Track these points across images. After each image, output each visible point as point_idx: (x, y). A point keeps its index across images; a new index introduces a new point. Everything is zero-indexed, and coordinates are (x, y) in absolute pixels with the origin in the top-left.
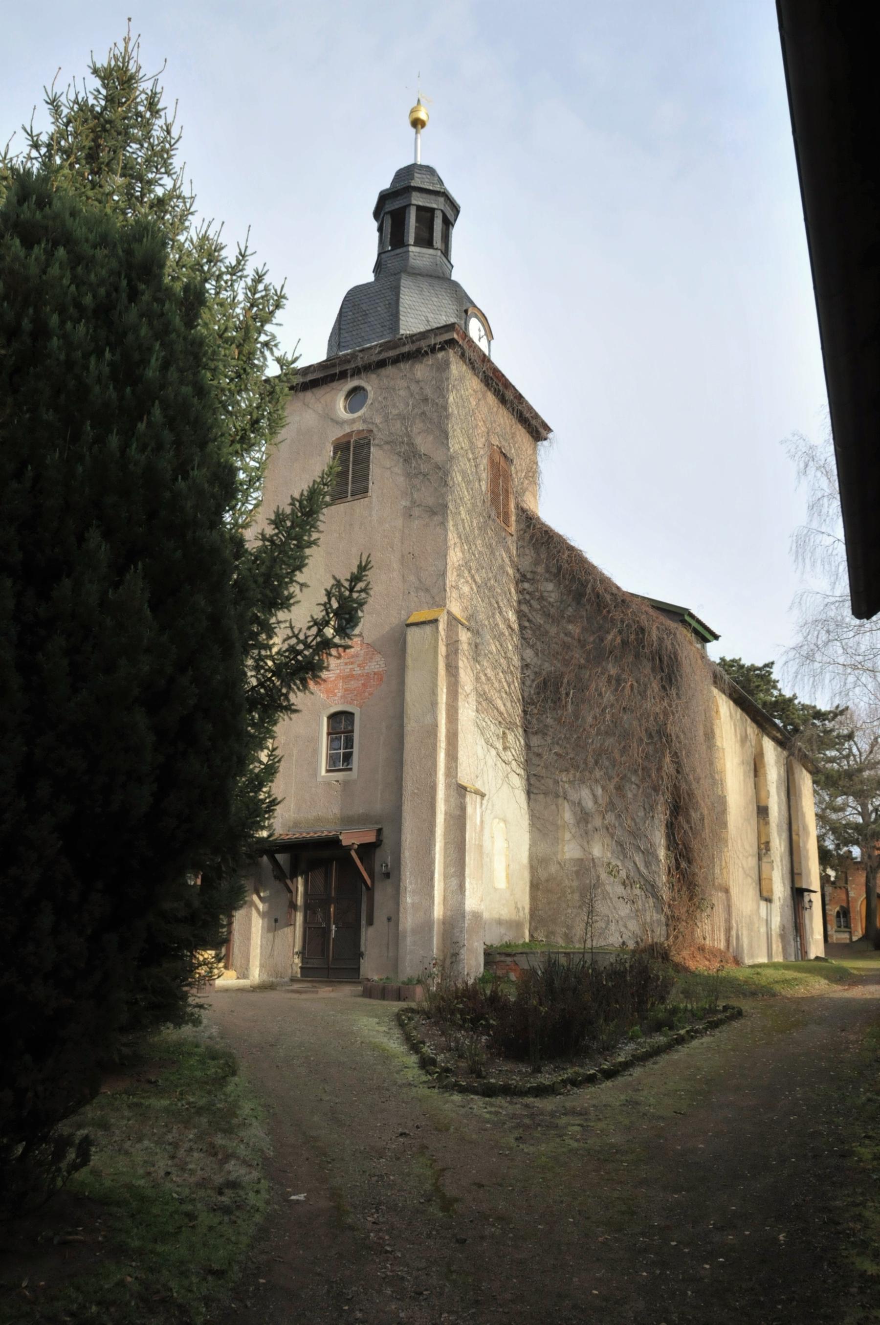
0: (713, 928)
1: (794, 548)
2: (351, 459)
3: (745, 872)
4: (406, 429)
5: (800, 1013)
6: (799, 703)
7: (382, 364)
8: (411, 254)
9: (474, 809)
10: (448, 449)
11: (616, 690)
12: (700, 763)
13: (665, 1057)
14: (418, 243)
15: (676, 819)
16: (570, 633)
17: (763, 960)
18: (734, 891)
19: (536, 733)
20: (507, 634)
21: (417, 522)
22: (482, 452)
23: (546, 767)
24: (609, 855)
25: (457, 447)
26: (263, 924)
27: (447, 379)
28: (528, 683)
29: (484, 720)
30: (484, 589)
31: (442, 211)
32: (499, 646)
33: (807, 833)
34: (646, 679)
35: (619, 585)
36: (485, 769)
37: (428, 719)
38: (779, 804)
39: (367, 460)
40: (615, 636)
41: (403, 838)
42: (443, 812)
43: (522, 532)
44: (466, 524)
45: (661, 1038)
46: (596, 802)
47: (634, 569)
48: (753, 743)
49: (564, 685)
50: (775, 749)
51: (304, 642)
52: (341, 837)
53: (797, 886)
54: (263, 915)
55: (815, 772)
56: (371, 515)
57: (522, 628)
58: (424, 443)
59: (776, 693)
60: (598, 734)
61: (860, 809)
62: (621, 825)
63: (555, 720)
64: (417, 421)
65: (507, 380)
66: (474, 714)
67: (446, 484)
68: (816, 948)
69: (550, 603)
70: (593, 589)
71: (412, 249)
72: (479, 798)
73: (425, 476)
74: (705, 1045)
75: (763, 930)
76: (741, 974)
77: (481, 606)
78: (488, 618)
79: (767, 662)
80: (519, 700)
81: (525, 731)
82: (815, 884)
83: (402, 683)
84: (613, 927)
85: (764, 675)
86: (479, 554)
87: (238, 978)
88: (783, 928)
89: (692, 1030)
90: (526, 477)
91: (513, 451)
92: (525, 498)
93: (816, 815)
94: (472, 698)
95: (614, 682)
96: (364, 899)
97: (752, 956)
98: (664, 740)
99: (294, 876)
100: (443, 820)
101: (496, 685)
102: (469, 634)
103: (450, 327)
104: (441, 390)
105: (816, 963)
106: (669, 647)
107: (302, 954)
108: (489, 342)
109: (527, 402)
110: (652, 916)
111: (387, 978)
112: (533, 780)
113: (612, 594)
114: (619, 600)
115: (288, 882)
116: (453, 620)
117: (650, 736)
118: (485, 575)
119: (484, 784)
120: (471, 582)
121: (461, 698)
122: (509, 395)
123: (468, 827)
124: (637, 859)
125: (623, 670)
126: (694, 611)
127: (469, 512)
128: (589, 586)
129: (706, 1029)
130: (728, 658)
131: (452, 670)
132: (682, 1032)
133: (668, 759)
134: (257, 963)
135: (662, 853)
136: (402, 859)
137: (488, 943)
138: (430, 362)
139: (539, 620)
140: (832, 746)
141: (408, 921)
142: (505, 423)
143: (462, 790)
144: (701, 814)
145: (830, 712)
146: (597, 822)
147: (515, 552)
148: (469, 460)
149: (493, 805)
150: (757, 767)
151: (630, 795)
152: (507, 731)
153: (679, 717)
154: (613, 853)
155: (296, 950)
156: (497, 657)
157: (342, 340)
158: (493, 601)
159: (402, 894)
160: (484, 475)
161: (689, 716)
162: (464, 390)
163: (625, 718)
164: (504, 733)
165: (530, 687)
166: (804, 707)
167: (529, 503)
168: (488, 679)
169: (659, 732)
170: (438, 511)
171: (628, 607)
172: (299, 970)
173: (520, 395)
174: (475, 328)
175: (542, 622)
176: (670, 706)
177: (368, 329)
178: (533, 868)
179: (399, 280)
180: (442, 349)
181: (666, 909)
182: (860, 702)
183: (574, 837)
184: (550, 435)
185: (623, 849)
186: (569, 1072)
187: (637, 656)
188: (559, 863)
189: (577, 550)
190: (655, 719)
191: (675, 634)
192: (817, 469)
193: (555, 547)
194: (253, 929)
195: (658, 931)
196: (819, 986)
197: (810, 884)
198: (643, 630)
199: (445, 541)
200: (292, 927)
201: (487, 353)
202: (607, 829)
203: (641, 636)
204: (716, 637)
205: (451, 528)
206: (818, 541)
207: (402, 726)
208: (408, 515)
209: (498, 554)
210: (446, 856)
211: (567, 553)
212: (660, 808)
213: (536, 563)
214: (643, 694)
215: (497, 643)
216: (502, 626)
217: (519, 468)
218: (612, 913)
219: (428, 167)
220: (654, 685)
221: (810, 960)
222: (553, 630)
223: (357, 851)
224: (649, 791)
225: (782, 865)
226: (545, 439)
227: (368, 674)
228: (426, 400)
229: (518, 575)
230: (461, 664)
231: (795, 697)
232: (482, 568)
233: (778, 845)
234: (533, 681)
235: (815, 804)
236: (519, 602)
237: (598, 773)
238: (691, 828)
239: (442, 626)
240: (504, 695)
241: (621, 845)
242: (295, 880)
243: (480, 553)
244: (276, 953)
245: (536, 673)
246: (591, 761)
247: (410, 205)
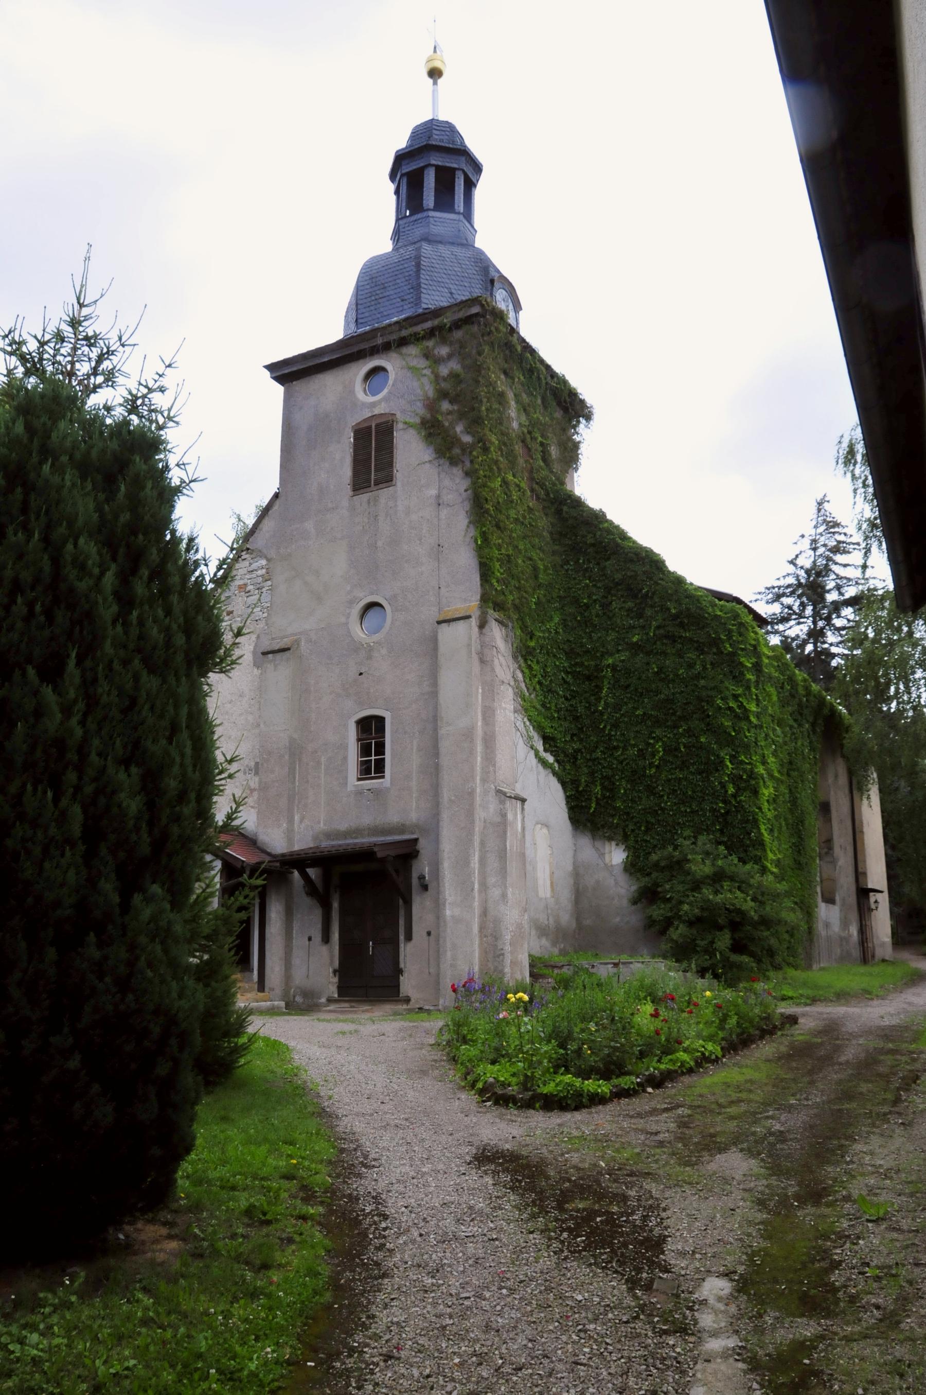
2: (373, 445)
14: (438, 207)
56: (396, 506)
72: (519, 803)
96: (402, 913)
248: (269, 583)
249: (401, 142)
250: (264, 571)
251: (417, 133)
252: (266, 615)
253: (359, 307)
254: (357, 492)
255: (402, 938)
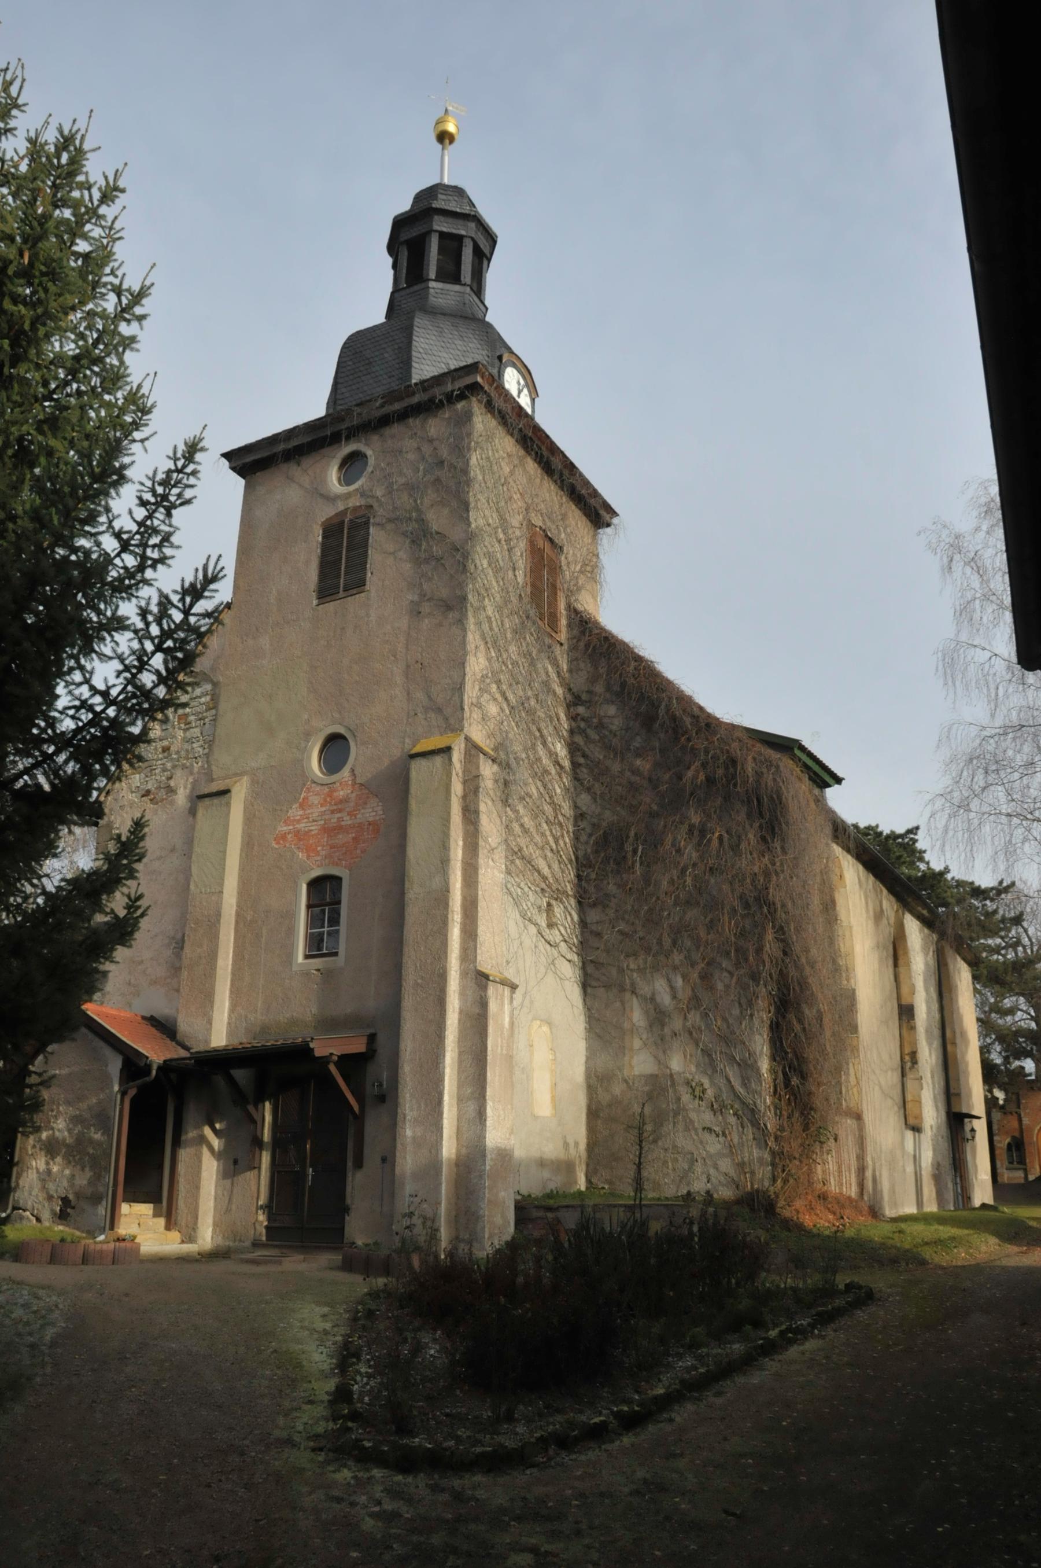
0: (840, 1167)
1: (940, 667)
2: (345, 544)
3: (883, 1092)
4: (415, 501)
5: (960, 1296)
6: (953, 878)
7: (384, 422)
8: (431, 291)
9: (500, 1007)
10: (469, 524)
11: (699, 844)
12: (815, 941)
13: (740, 1380)
14: (441, 277)
15: (784, 1017)
16: (638, 770)
17: (911, 1209)
18: (868, 1117)
19: (594, 905)
20: (553, 771)
21: (426, 621)
22: (518, 533)
23: (608, 951)
24: (693, 1069)
25: (481, 522)
26: (218, 1166)
27: (469, 435)
28: (584, 838)
29: (519, 886)
30: (519, 709)
31: (473, 239)
32: (542, 789)
33: (966, 1041)
34: (740, 829)
35: (702, 703)
36: (520, 952)
37: (437, 882)
38: (928, 1002)
39: (365, 544)
40: (697, 771)
41: (402, 1046)
42: (457, 1010)
43: (575, 641)
44: (494, 624)
45: (736, 1346)
46: (674, 997)
47: (727, 686)
48: (892, 920)
49: (631, 839)
50: (921, 931)
51: (105, 694)
52: (312, 1045)
53: (955, 1110)
54: (218, 1156)
55: (974, 963)
56: (368, 615)
57: (575, 765)
58: (437, 519)
59: (922, 866)
60: (676, 904)
61: (1033, 1014)
62: (708, 1026)
63: (619, 886)
64: (429, 492)
65: (552, 443)
66: (502, 876)
67: (465, 569)
68: (982, 1193)
69: (611, 732)
70: (668, 708)
71: (432, 284)
72: (507, 991)
73: (438, 560)
74: (807, 1355)
75: (910, 1169)
76: (877, 1232)
77: (514, 732)
78: (526, 749)
79: (910, 827)
80: (570, 861)
81: (579, 903)
82: (978, 1108)
83: (403, 836)
84: (699, 1168)
85: (908, 843)
86: (512, 664)
87: (183, 1242)
88: (937, 1166)
89: (789, 1330)
90: (581, 572)
91: (563, 535)
92: (580, 598)
93: (979, 1020)
94: (500, 855)
95: (696, 833)
96: (351, 1131)
97: (895, 1205)
98: (765, 910)
99: (259, 1100)
100: (456, 1021)
101: (538, 839)
102: (495, 768)
103: (472, 368)
104: (460, 449)
105: (981, 1213)
106: (770, 783)
107: (268, 1208)
108: (533, 400)
109: (581, 475)
110: (751, 1153)
111: (376, 1243)
112: (590, 969)
113: (693, 716)
114: (703, 724)
115: (251, 1108)
116: (473, 749)
117: (747, 906)
118: (521, 693)
119: (518, 972)
120: (500, 697)
121: (482, 853)
122: (556, 463)
123: (491, 1030)
124: (731, 1074)
125: (709, 816)
126: (806, 743)
127: (499, 609)
128: (663, 707)
129: (813, 1326)
130: (862, 825)
131: (471, 815)
132: (773, 1333)
133: (770, 936)
134: (210, 1220)
135: (765, 1065)
136: (401, 1074)
137: (525, 1192)
138: (447, 416)
139: (598, 754)
140: (994, 934)
141: (408, 1162)
142: (552, 500)
143: (482, 979)
144: (819, 1011)
145: (992, 889)
146: (677, 1024)
147: (565, 667)
148: (499, 541)
149: (532, 1002)
150: (896, 951)
151: (720, 986)
152: (554, 902)
153: (785, 879)
154: (697, 1066)
155: (260, 1203)
156: (538, 803)
157: (338, 397)
158: (534, 728)
159: (400, 1124)
160: (521, 564)
161: (798, 877)
162: (492, 450)
163: (713, 881)
164: (549, 905)
165: (587, 843)
166: (960, 884)
167: (585, 603)
168: (526, 831)
169: (757, 899)
170: (454, 606)
171: (715, 733)
172: (264, 1231)
173: (572, 464)
174: (511, 379)
175: (601, 757)
176: (774, 864)
177: (371, 381)
178: (591, 1089)
179: (412, 319)
180: (462, 397)
181: (771, 1143)
182: (1030, 875)
183: (645, 1045)
184: (615, 520)
185: (712, 1060)
186: (556, 1423)
187: (727, 798)
188: (626, 1081)
189: (647, 661)
190: (753, 881)
191: (778, 767)
192: (965, 564)
193: (618, 658)
194: (204, 1174)
195: (759, 1175)
196: (986, 1248)
197: (970, 1106)
198: (734, 762)
199: (464, 643)
200: (256, 1171)
201: (529, 411)
202: (691, 1033)
203: (731, 770)
204: (839, 780)
205: (472, 626)
206: (969, 658)
207: (402, 894)
208: (416, 613)
209: (539, 666)
210: (461, 1070)
211: (633, 664)
212: (761, 1003)
213: (593, 680)
214: (735, 848)
215: (539, 784)
216: (545, 761)
217: (570, 559)
218: (697, 1148)
219: (456, 187)
220: (751, 836)
221: (975, 1209)
222: (616, 767)
223: (336, 1064)
224: (746, 980)
225: (933, 1083)
226: (608, 525)
227: (360, 825)
228: (441, 463)
229: (569, 697)
230: (482, 807)
231: (947, 870)
232: (517, 683)
233: (928, 1056)
234: (590, 835)
235: (977, 1005)
236: (571, 732)
237: (677, 958)
238: (804, 1029)
239: (457, 756)
240: (549, 854)
241: (709, 1055)
242: (260, 1106)
243: (515, 663)
244: (234, 1207)
245: (594, 825)
246: (667, 942)
247: (430, 232)
248: (213, 712)
249: (405, 205)
250: (208, 698)
251: (419, 197)
252: (206, 751)
253: (339, 386)
254: (323, 600)
255: (350, 1164)
